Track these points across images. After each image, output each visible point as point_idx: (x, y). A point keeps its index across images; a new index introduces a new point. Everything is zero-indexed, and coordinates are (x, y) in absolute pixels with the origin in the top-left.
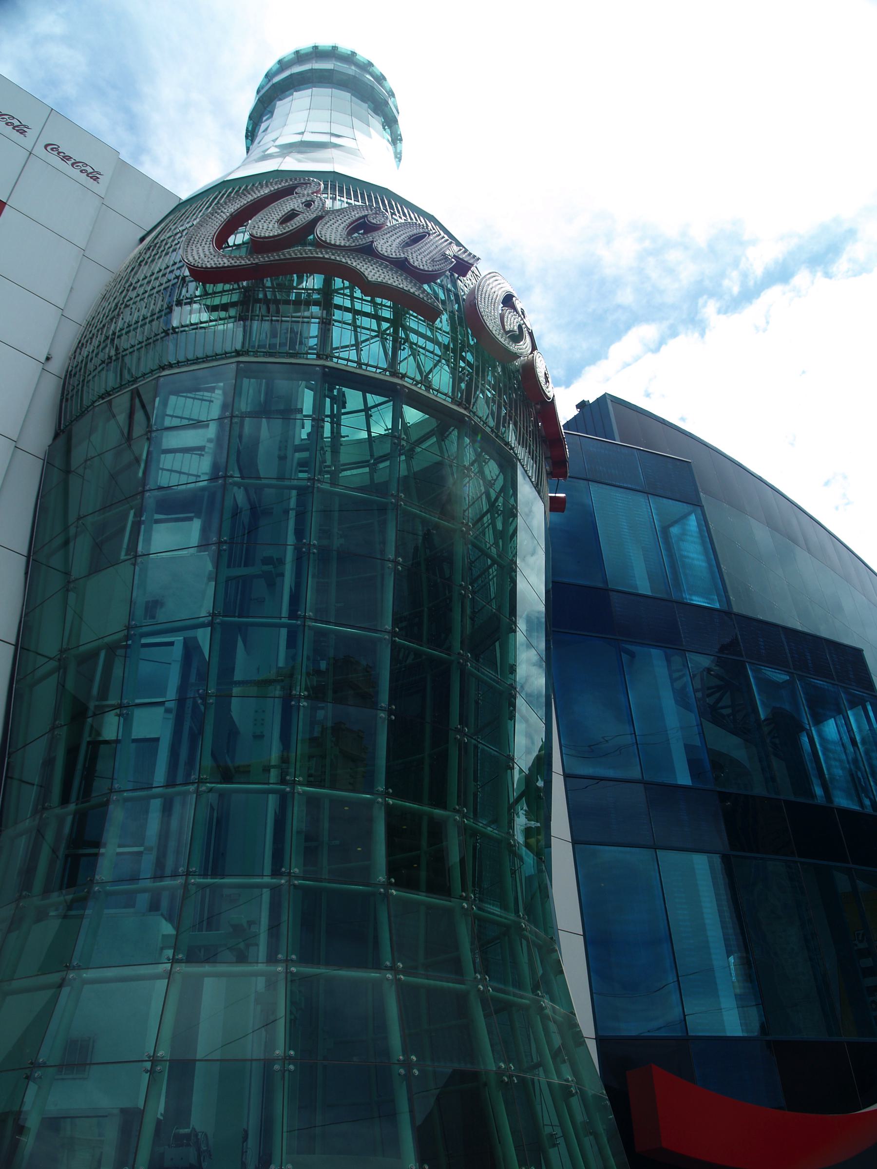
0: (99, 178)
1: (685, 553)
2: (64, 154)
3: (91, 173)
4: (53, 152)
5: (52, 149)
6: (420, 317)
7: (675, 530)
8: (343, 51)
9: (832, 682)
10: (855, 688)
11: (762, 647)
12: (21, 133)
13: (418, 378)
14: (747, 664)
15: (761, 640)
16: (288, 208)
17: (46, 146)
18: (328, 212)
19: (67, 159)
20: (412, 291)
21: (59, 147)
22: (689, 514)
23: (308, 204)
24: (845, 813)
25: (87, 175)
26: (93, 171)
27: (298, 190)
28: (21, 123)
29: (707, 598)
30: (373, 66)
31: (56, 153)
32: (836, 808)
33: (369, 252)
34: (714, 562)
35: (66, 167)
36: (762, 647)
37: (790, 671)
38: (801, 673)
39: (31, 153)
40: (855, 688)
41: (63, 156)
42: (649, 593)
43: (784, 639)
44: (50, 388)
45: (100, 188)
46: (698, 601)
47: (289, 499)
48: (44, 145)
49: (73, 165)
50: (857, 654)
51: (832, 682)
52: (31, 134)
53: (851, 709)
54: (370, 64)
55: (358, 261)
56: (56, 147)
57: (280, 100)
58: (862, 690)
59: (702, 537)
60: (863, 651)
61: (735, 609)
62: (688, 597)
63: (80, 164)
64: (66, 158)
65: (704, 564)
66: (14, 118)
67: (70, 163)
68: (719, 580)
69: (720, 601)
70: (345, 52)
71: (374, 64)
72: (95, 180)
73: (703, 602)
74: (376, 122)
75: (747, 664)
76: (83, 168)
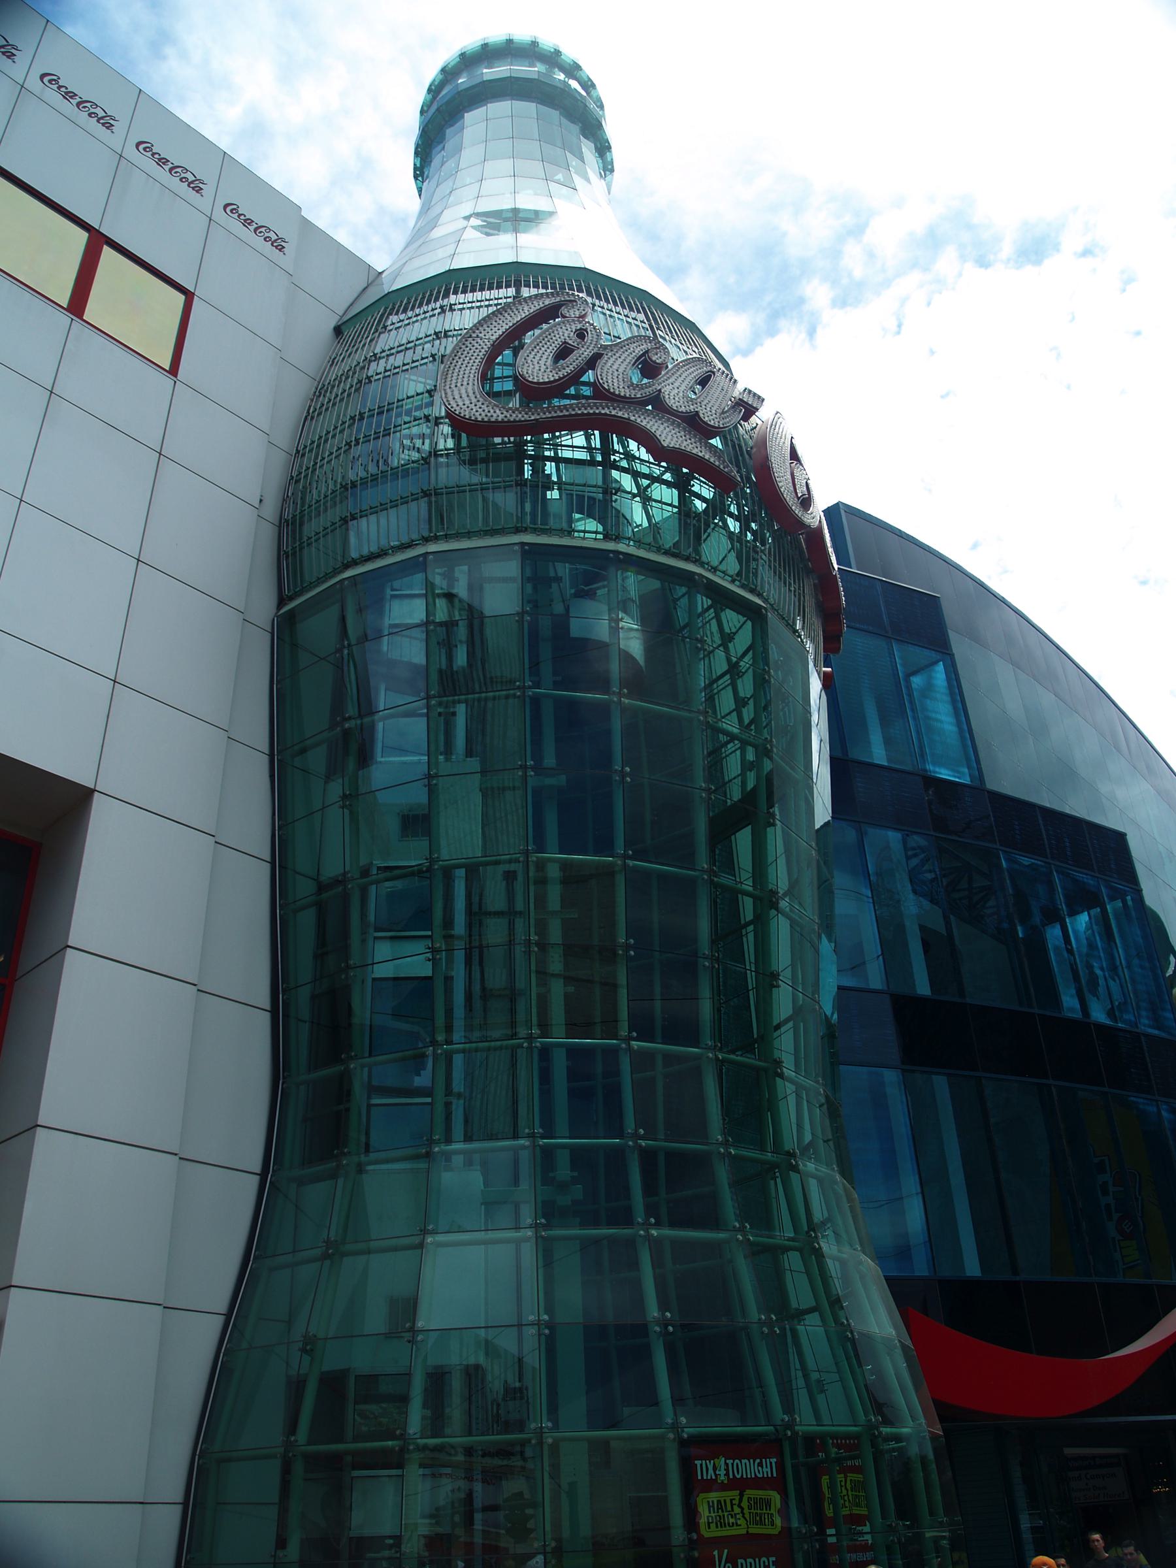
0: (202, 189)
1: (933, 715)
2: (67, 88)
3: (102, 118)
4: (145, 153)
5: (50, 81)
6: (701, 478)
7: (917, 681)
8: (545, 47)
9: (1093, 874)
10: (1116, 881)
11: (1017, 832)
12: (9, 57)
13: (635, 491)
14: (1001, 852)
15: (1017, 823)
16: (672, 443)
17: (42, 77)
18: (605, 347)
19: (71, 97)
20: (707, 457)
21: (59, 78)
22: (936, 663)
23: (581, 334)
24: (1100, 1027)
25: (98, 121)
26: (105, 115)
27: (564, 310)
28: (7, 42)
29: (953, 770)
30: (581, 70)
31: (55, 87)
32: (1094, 1024)
33: (658, 404)
34: (965, 727)
35: (247, 234)
36: (1017, 832)
37: (1047, 861)
38: (1058, 863)
39: (210, 220)
40: (1116, 881)
41: (65, 92)
42: (885, 764)
43: (1041, 822)
44: (268, 534)
45: (282, 261)
46: (945, 774)
47: (538, 664)
48: (40, 74)
49: (78, 104)
50: (1118, 841)
51: (1093, 874)
52: (208, 190)
53: (1109, 903)
54: (578, 67)
55: (648, 419)
56: (55, 78)
57: (467, 112)
58: (1123, 883)
59: (952, 694)
60: (1126, 835)
61: (991, 785)
62: (932, 768)
63: (88, 105)
64: (69, 95)
65: (954, 729)
66: (187, 170)
67: (74, 102)
68: (971, 749)
69: (971, 776)
70: (548, 49)
71: (583, 67)
72: (107, 128)
73: (949, 775)
74: (588, 149)
75: (1001, 852)
76: (183, 175)
